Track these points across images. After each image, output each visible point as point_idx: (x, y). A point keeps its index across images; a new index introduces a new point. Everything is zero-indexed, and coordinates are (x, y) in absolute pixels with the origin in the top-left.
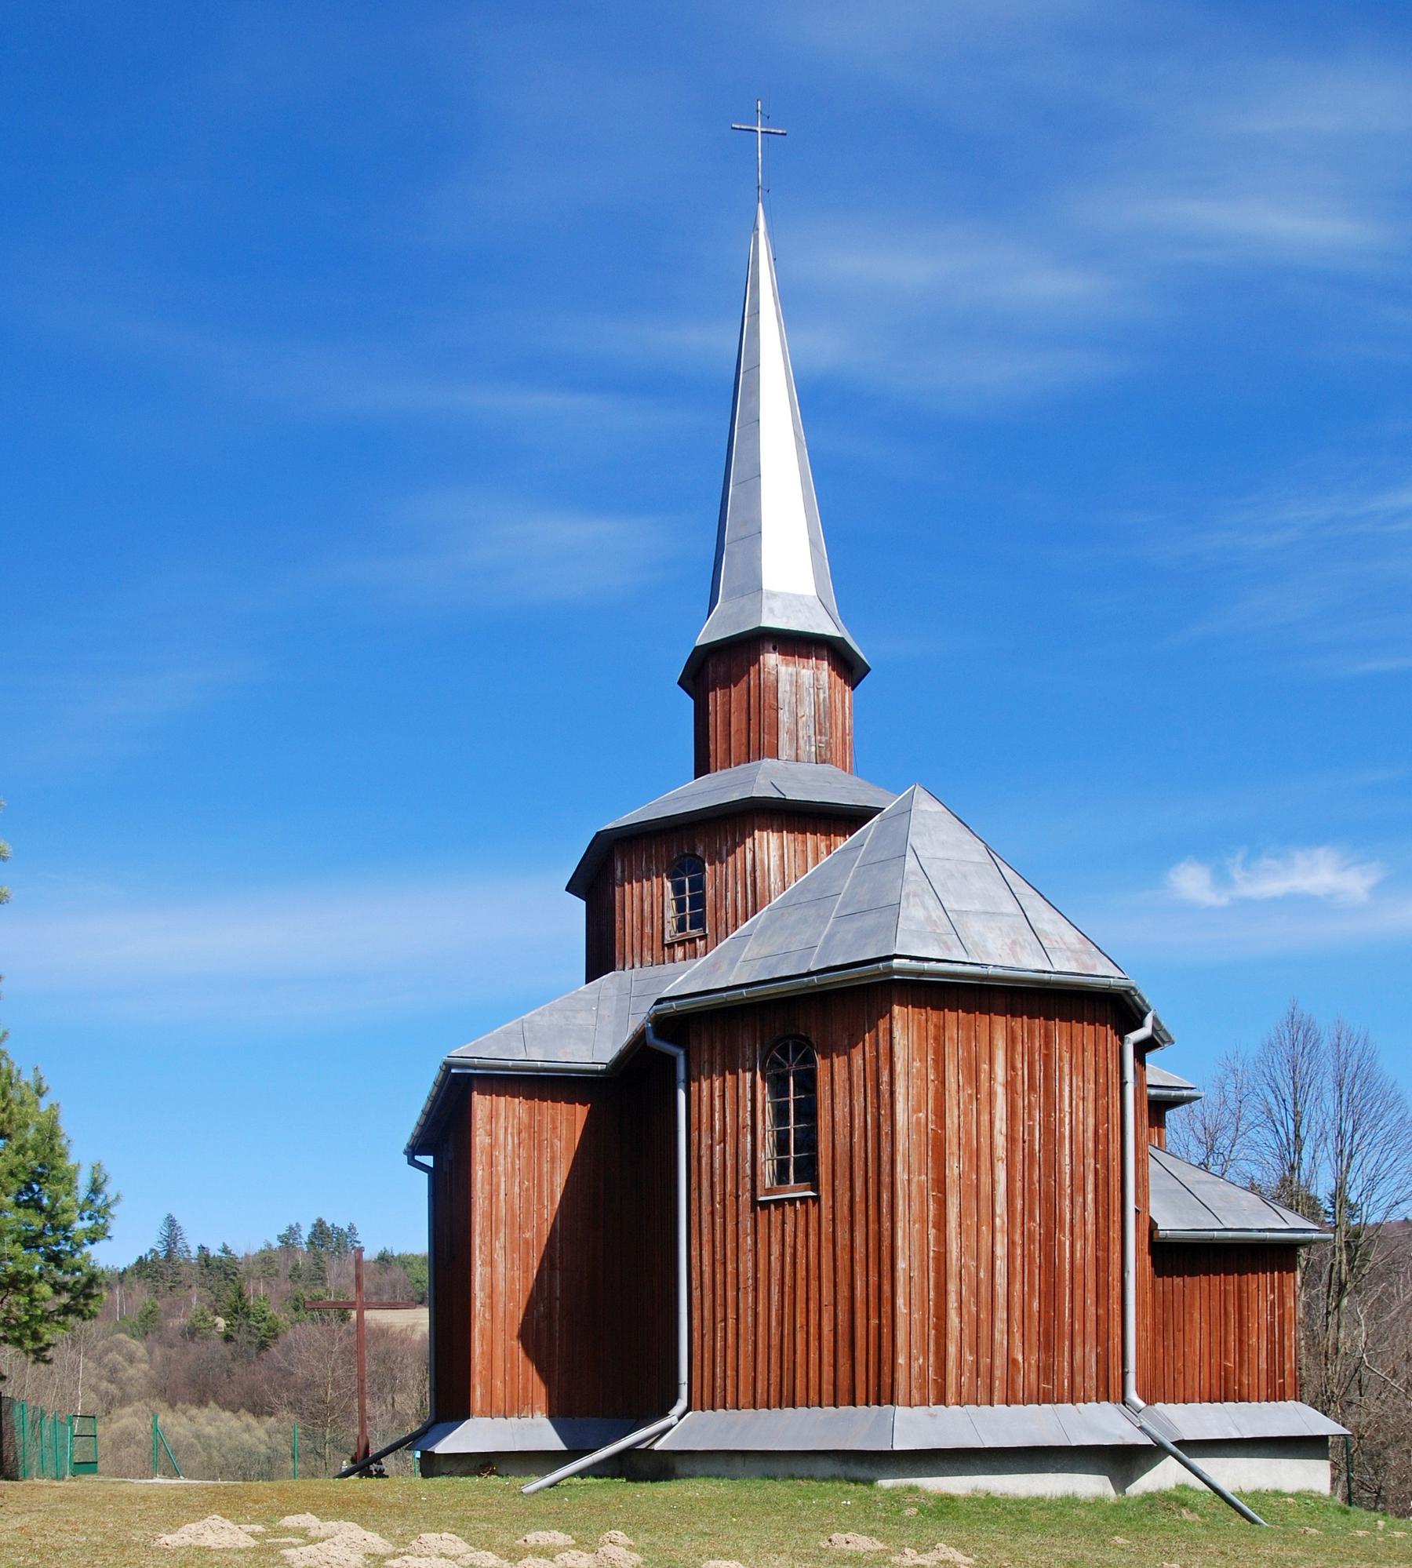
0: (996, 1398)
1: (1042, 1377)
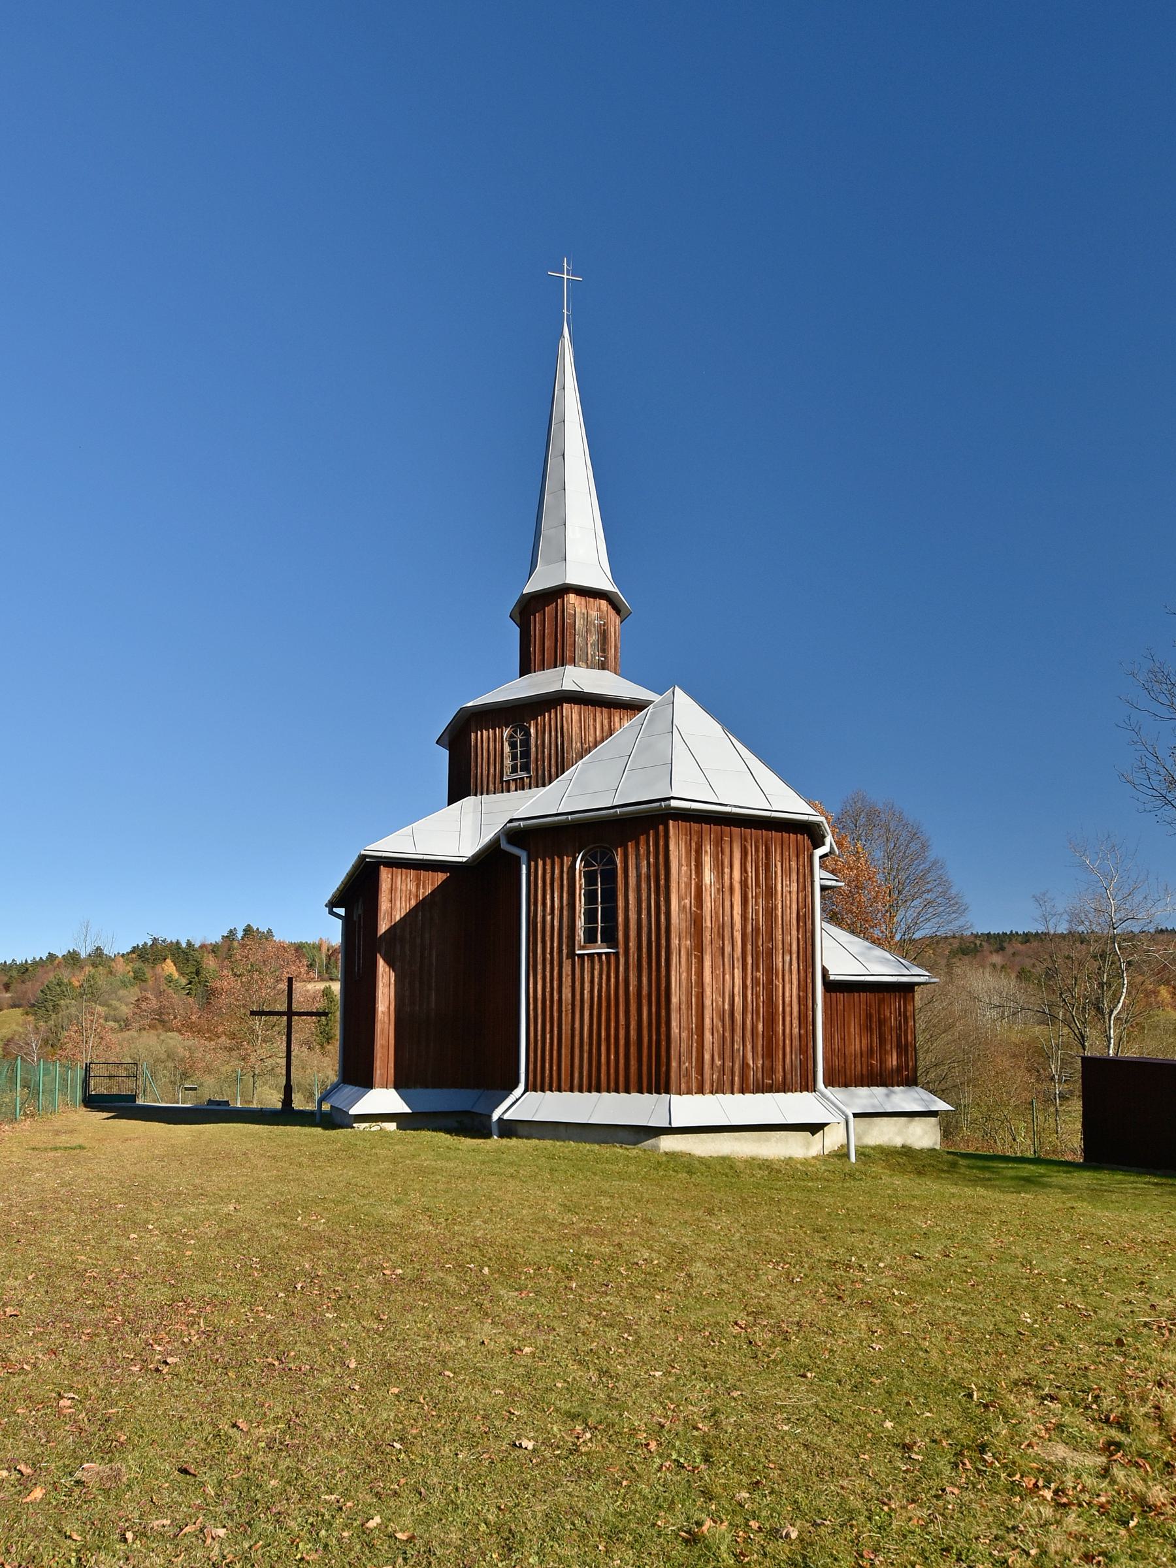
0: (735, 1089)
1: (765, 1075)
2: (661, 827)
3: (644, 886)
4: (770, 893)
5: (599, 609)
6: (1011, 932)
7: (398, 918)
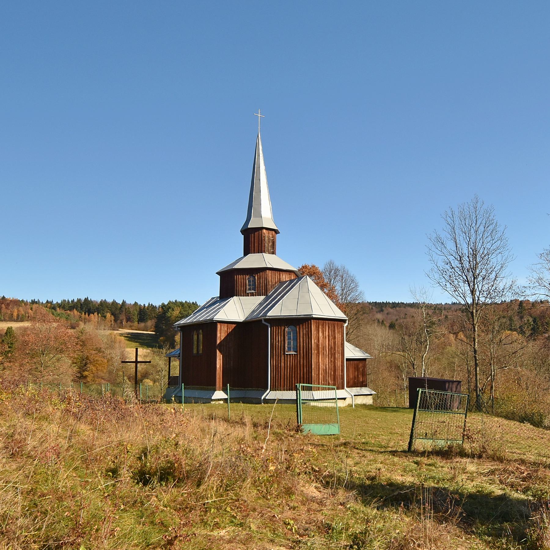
2: (309, 321)
3: (305, 336)
4: (335, 338)
5: (272, 234)
6: (387, 302)
7: (222, 339)
